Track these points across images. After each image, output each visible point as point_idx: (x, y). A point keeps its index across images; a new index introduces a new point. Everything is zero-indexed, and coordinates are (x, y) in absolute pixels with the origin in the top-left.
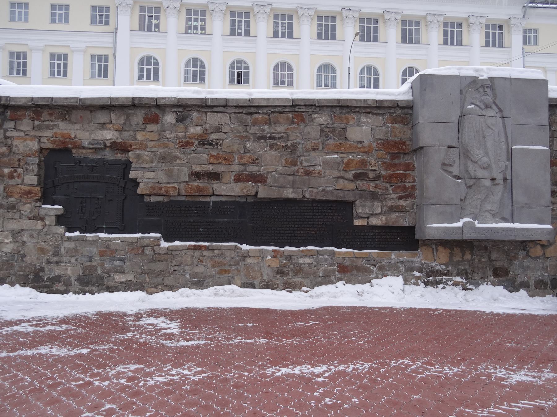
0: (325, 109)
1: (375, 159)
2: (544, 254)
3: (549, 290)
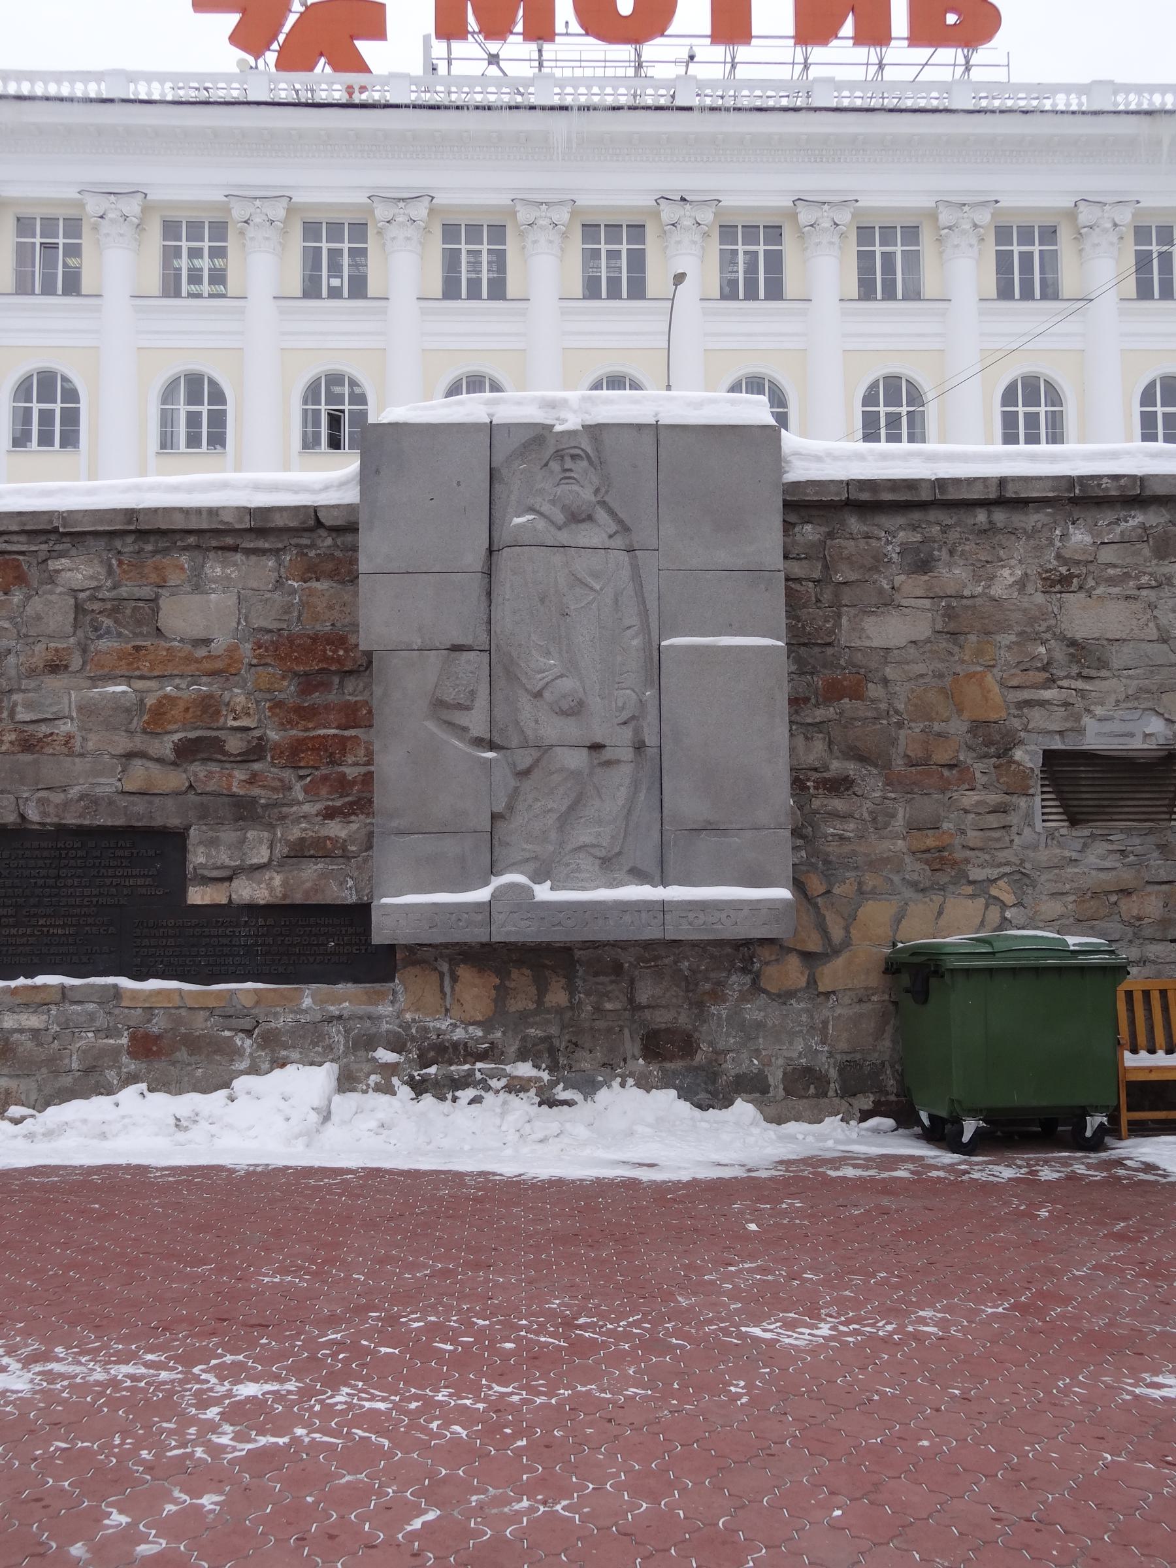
0: (91, 541)
1: (248, 695)
2: (812, 982)
3: (837, 1100)
